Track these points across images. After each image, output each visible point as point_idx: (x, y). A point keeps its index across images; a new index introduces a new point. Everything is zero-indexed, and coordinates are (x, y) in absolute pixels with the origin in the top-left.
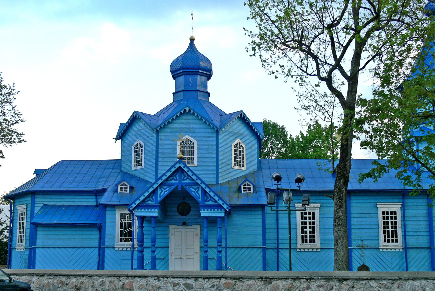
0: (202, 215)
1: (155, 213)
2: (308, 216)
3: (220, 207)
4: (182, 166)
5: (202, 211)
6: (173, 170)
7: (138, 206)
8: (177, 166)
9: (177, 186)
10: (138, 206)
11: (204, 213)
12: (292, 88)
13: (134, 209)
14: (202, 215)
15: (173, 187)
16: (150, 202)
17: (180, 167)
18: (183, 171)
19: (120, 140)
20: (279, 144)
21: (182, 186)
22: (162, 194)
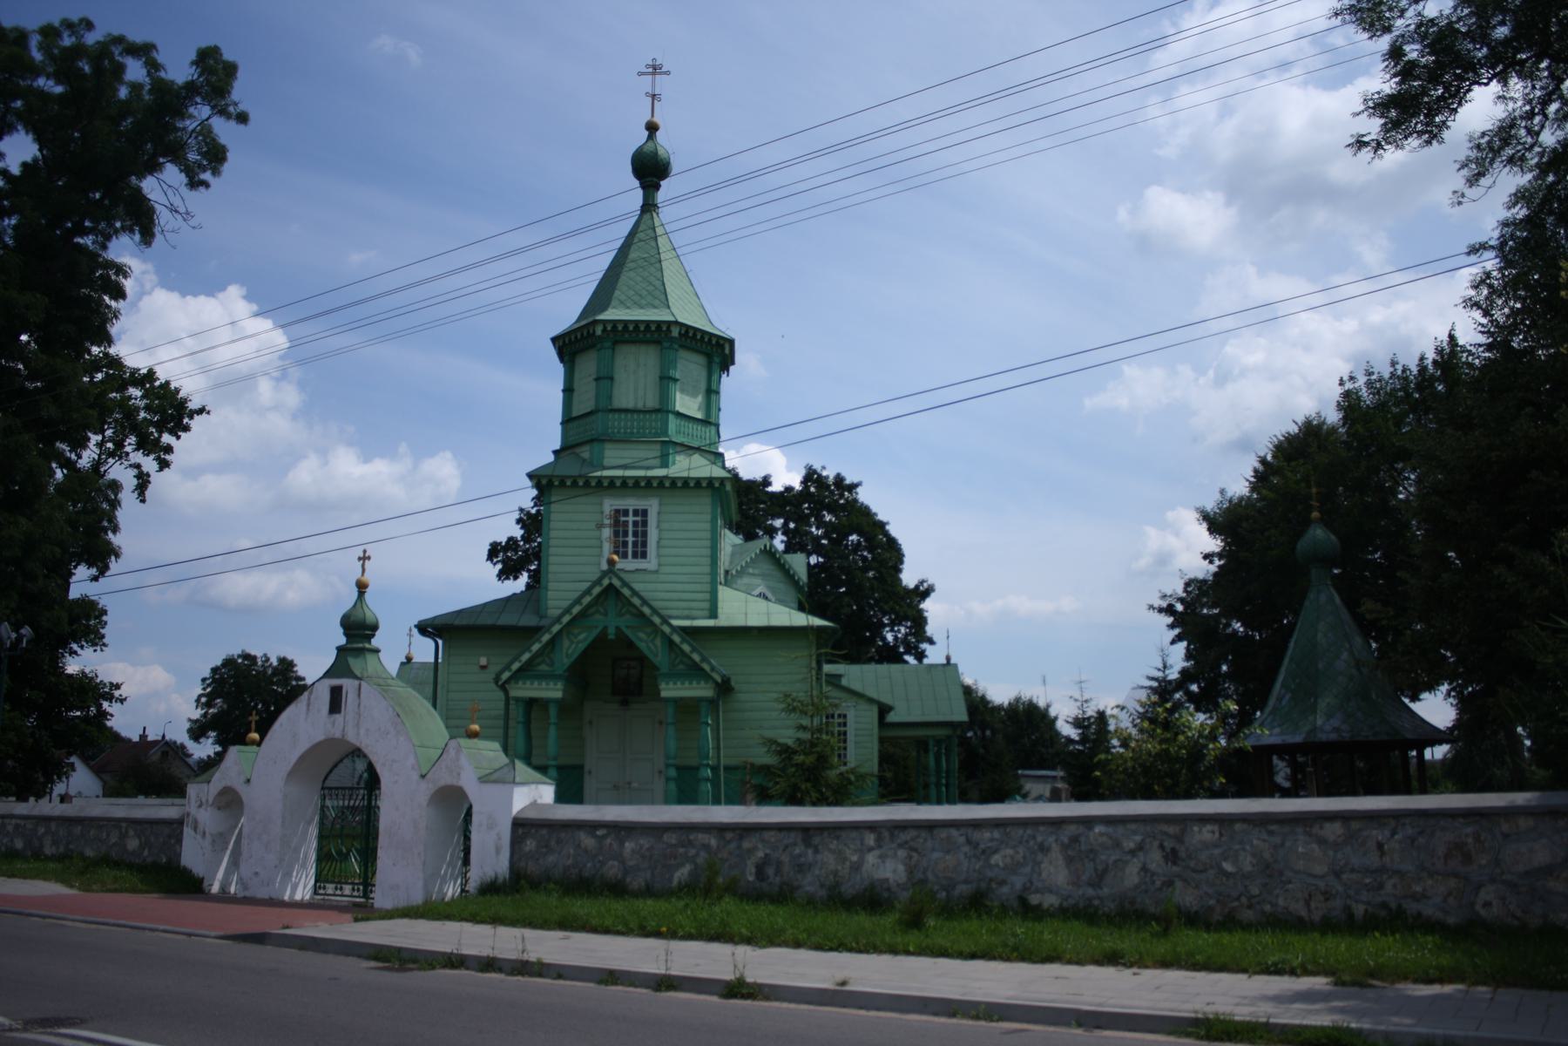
0: (664, 694)
1: (553, 691)
2: (837, 720)
3: (706, 676)
4: (616, 583)
5: (663, 686)
6: (597, 590)
7: (516, 676)
8: (606, 582)
9: (605, 628)
10: (516, 676)
11: (669, 690)
12: (650, 170)
13: (508, 681)
14: (664, 694)
15: (595, 633)
16: (544, 667)
17: (611, 585)
18: (618, 593)
19: (964, 717)
20: (818, 550)
21: (618, 628)
22: (571, 649)
